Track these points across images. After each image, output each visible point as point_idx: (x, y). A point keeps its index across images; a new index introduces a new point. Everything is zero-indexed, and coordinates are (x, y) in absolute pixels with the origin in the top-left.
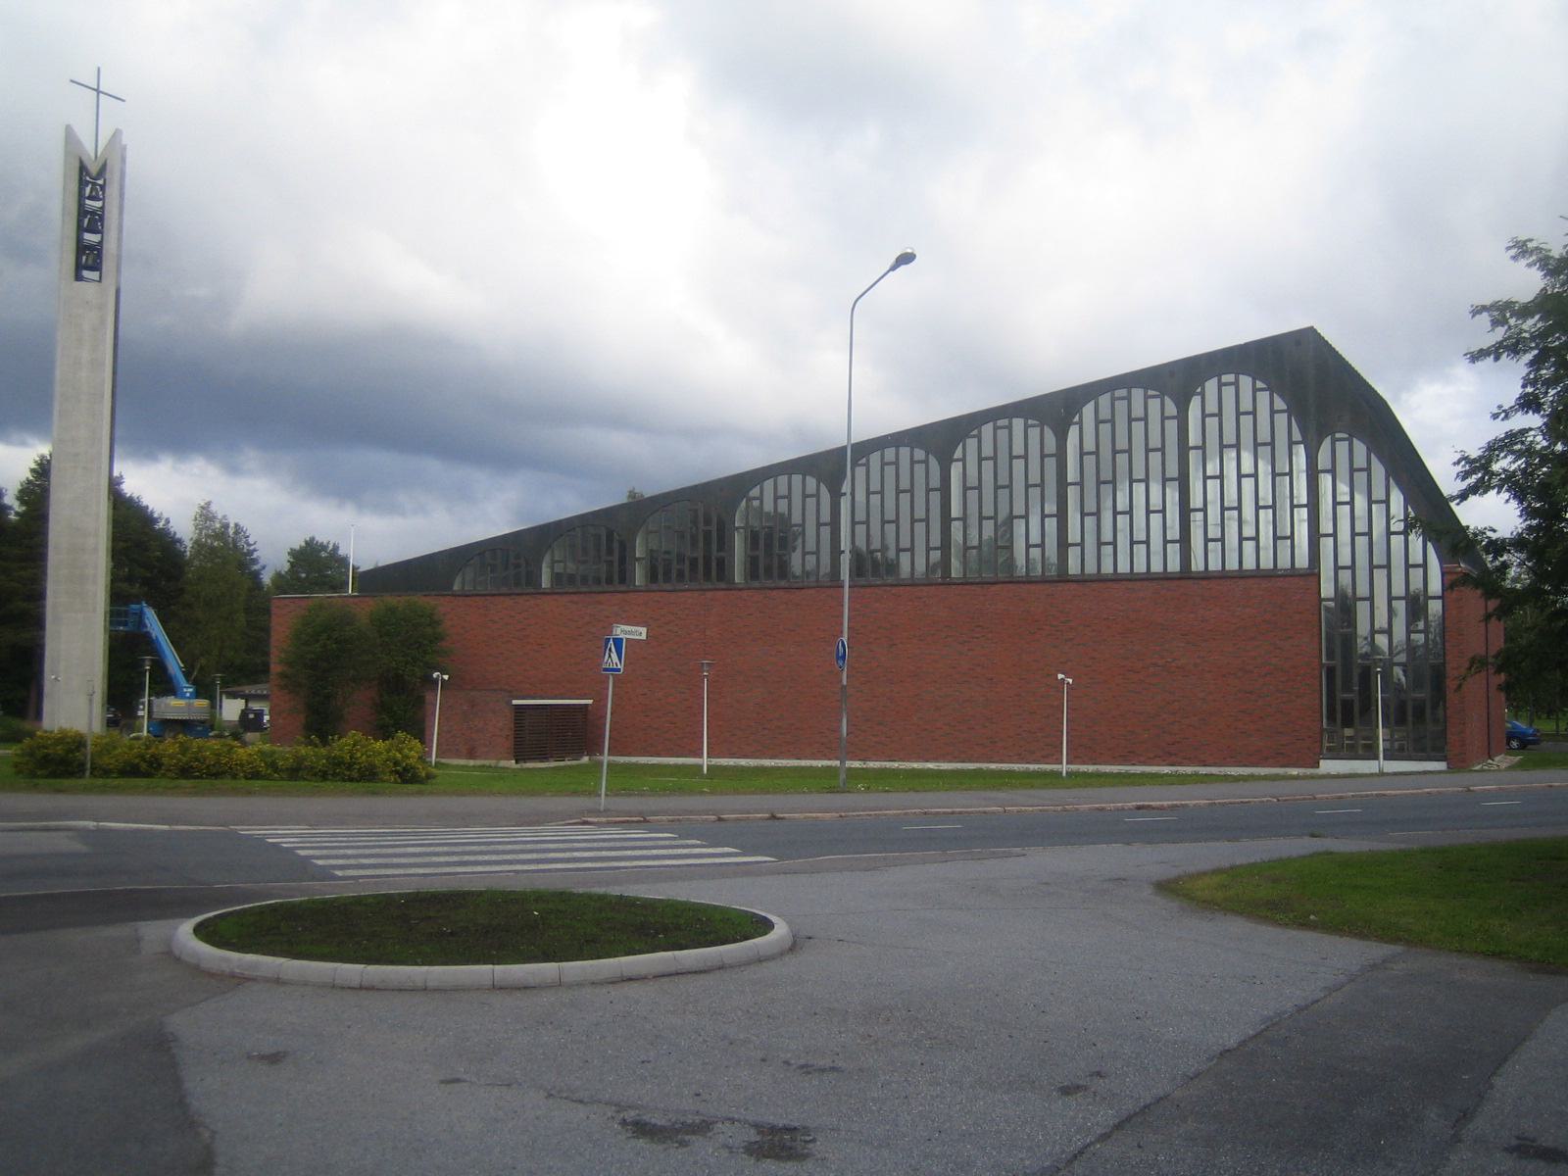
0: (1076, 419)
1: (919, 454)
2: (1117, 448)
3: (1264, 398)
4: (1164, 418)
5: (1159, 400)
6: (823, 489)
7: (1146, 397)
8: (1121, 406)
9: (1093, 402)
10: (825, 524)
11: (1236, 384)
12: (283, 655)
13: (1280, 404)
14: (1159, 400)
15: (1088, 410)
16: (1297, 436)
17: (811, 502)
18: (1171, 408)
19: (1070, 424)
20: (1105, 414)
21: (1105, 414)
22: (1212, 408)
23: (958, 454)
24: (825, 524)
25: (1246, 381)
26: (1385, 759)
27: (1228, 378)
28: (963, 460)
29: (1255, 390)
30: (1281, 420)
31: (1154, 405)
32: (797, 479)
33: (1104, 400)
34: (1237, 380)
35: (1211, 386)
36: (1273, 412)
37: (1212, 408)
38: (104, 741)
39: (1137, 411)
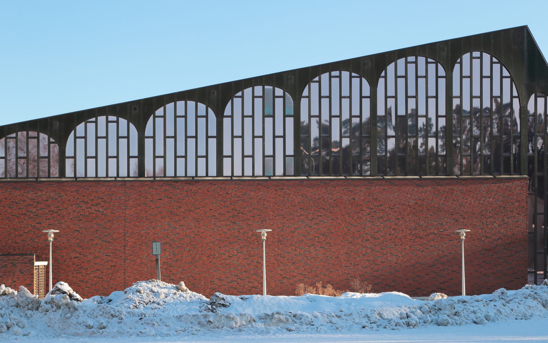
0: (459, 60)
1: (202, 107)
2: (251, 118)
3: (497, 67)
4: (437, 77)
5: (359, 79)
6: (211, 112)
7: (427, 63)
8: (412, 67)
9: (393, 63)
10: (456, 97)
11: (481, 58)
12: (325, 161)
13: (506, 73)
14: (359, 79)
15: (391, 68)
16: (515, 93)
17: (202, 121)
18: (442, 72)
19: (379, 76)
20: (401, 72)
21: (401, 72)
22: (466, 72)
23: (305, 93)
24: (456, 97)
25: (486, 57)
26: (469, 293)
27: (476, 54)
28: (309, 97)
29: (492, 63)
30: (507, 82)
31: (432, 67)
32: (191, 104)
33: (401, 62)
34: (481, 55)
35: (466, 57)
36: (502, 77)
37: (466, 72)
38: (330, 331)
39: (422, 72)
